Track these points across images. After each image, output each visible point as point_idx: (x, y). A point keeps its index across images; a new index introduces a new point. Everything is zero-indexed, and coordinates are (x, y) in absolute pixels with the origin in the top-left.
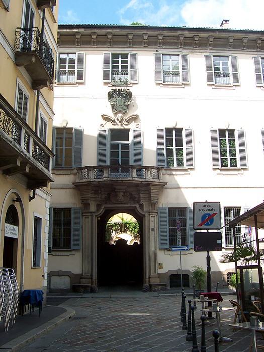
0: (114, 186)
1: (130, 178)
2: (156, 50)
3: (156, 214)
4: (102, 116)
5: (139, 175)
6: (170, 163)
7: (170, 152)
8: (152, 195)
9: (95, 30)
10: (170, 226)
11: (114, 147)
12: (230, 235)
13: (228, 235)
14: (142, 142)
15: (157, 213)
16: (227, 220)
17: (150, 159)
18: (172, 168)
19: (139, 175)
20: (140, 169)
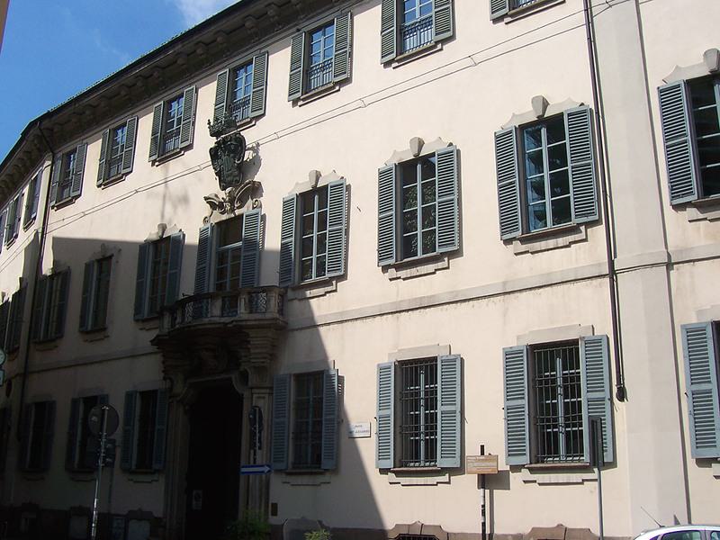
0: (246, 331)
1: (206, 320)
2: (294, 29)
3: (268, 391)
4: (206, 199)
5: (252, 307)
6: (305, 269)
7: (305, 247)
8: (252, 351)
9: (195, 38)
10: (566, 397)
11: (222, 257)
12: (555, 426)
13: (548, 427)
14: (259, 237)
15: (271, 388)
16: (547, 382)
17: (270, 275)
18: (308, 281)
19: (252, 307)
20: (255, 292)
